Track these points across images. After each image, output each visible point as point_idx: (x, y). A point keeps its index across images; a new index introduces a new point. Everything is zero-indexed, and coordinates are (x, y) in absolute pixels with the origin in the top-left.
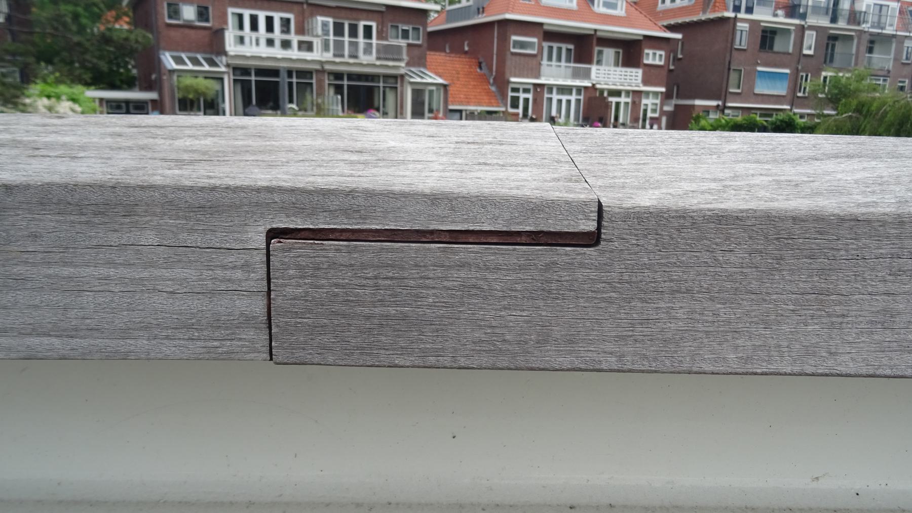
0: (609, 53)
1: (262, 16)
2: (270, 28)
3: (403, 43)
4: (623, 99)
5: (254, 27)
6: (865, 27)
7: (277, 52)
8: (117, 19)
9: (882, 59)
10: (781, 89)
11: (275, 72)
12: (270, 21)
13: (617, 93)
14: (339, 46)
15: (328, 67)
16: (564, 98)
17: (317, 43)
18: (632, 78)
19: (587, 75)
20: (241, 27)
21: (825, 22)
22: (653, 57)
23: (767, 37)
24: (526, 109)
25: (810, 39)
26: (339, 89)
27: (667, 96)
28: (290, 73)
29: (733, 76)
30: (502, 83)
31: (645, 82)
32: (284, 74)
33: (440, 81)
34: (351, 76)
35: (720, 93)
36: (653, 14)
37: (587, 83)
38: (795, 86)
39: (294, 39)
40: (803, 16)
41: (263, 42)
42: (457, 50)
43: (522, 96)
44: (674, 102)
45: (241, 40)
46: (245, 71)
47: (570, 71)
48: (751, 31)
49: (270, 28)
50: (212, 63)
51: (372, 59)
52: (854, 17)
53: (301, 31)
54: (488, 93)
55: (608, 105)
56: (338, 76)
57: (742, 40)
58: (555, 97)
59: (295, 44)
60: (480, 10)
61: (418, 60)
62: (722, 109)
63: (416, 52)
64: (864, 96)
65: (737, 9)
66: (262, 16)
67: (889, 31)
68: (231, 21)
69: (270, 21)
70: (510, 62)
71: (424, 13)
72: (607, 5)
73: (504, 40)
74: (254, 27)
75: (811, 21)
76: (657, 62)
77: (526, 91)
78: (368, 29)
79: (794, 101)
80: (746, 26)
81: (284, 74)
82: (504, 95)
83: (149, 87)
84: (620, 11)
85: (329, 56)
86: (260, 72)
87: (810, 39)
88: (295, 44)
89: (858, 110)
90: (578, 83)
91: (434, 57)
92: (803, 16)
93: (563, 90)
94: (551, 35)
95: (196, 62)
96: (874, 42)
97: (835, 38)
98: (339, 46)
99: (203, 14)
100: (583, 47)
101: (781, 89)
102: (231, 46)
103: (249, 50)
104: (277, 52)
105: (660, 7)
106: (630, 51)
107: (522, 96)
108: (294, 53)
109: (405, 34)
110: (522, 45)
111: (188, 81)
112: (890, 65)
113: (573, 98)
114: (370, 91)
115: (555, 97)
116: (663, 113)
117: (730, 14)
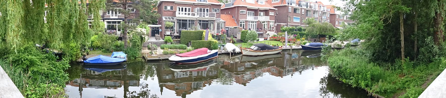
0: (262, 13)
1: (184, 8)
2: (186, 11)
3: (215, 13)
4: (265, 23)
5: (182, 10)
6: (313, 9)
7: (187, 16)
8: (155, 9)
9: (316, 15)
10: (298, 21)
11: (186, 21)
12: (186, 9)
13: (264, 22)
14: (201, 14)
15: (198, 19)
16: (252, 24)
17: (196, 14)
18: (267, 18)
19: (257, 18)
20: (179, 11)
21: (305, 8)
22: (271, 14)
23: (295, 10)
24: (243, 26)
25: (303, 11)
26: (200, 24)
27: (275, 22)
28: (189, 21)
29: (289, 18)
30: (238, 21)
31: (270, 19)
32: (188, 21)
33: (223, 21)
34: (203, 21)
35: (286, 22)
36: (271, 4)
37: (257, 20)
38: (301, 21)
39: (191, 13)
40: (301, 6)
41: (184, 14)
42: (228, 14)
43: (243, 23)
44: (277, 23)
45: (179, 13)
46: (180, 20)
47: (277, 72)
48: (292, 9)
49: (186, 11)
50: (173, 19)
51: (208, 17)
52: (311, 7)
53: (192, 11)
54: (235, 23)
55: (262, 25)
56: (200, 21)
57: (290, 10)
58: (250, 24)
59: (191, 14)
60: (233, 4)
61: (219, 17)
62: (287, 25)
63: (218, 15)
64: (314, 23)
65: (288, 4)
66: (184, 8)
67: (317, 10)
68: (178, 9)
69: (186, 9)
70: (240, 16)
71: (220, 5)
72: (261, 2)
73: (238, 11)
74: (182, 10)
75: (303, 7)
76: (272, 15)
77: (243, 22)
78: (207, 10)
79: (301, 24)
80: (291, 8)
81: (188, 21)
82: (238, 24)
83: (160, 24)
84: (264, 4)
85: (198, 16)
86: (183, 20)
87: (303, 11)
88: (191, 14)
89: (313, 26)
90: (255, 20)
91: (222, 16)
92: (301, 6)
93: (252, 22)
94: (249, 10)
95: (170, 19)
96: (314, 12)
97: (307, 11)
98: (201, 14)
99: (172, 8)
100: (256, 12)
101: (298, 21)
102: (177, 15)
103: (181, 16)
104: (187, 16)
105: (272, 2)
106: (266, 12)
107: (243, 23)
108: (190, 16)
109: (216, 11)
110: (242, 12)
111: (168, 23)
112: (318, 16)
113: (254, 24)
114: (207, 24)
115: (250, 24)
116: (275, 26)
117: (287, 5)
